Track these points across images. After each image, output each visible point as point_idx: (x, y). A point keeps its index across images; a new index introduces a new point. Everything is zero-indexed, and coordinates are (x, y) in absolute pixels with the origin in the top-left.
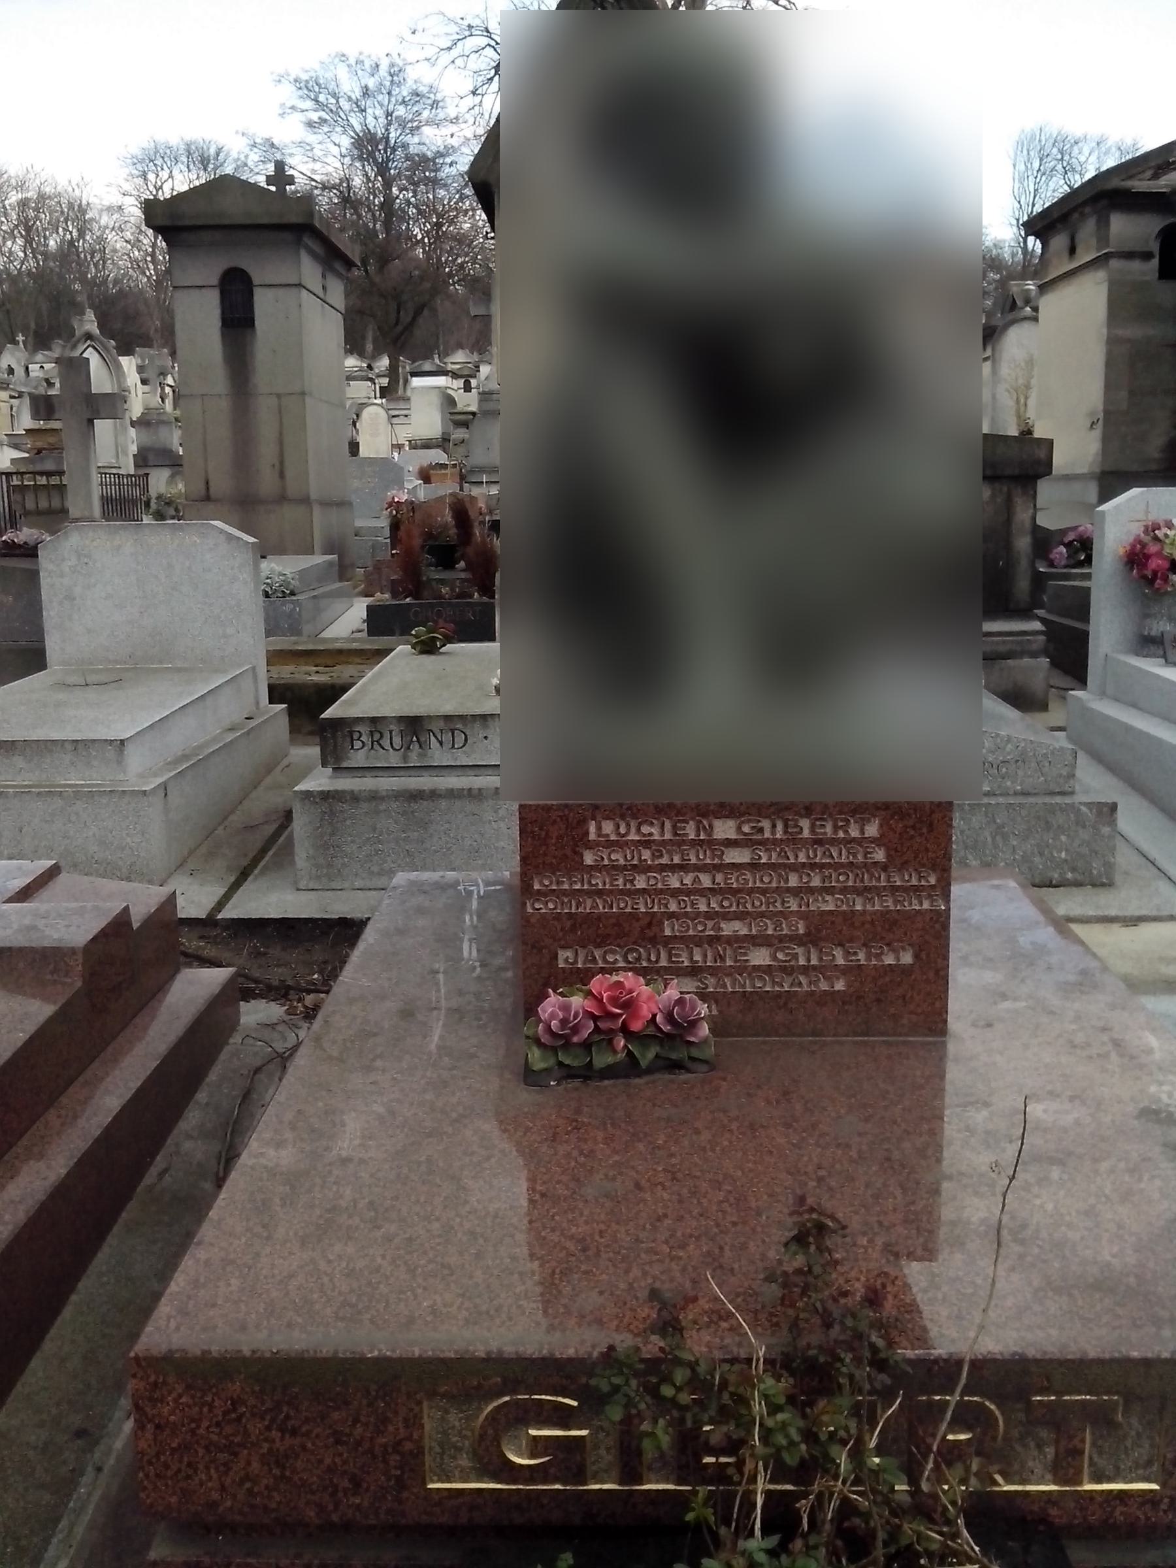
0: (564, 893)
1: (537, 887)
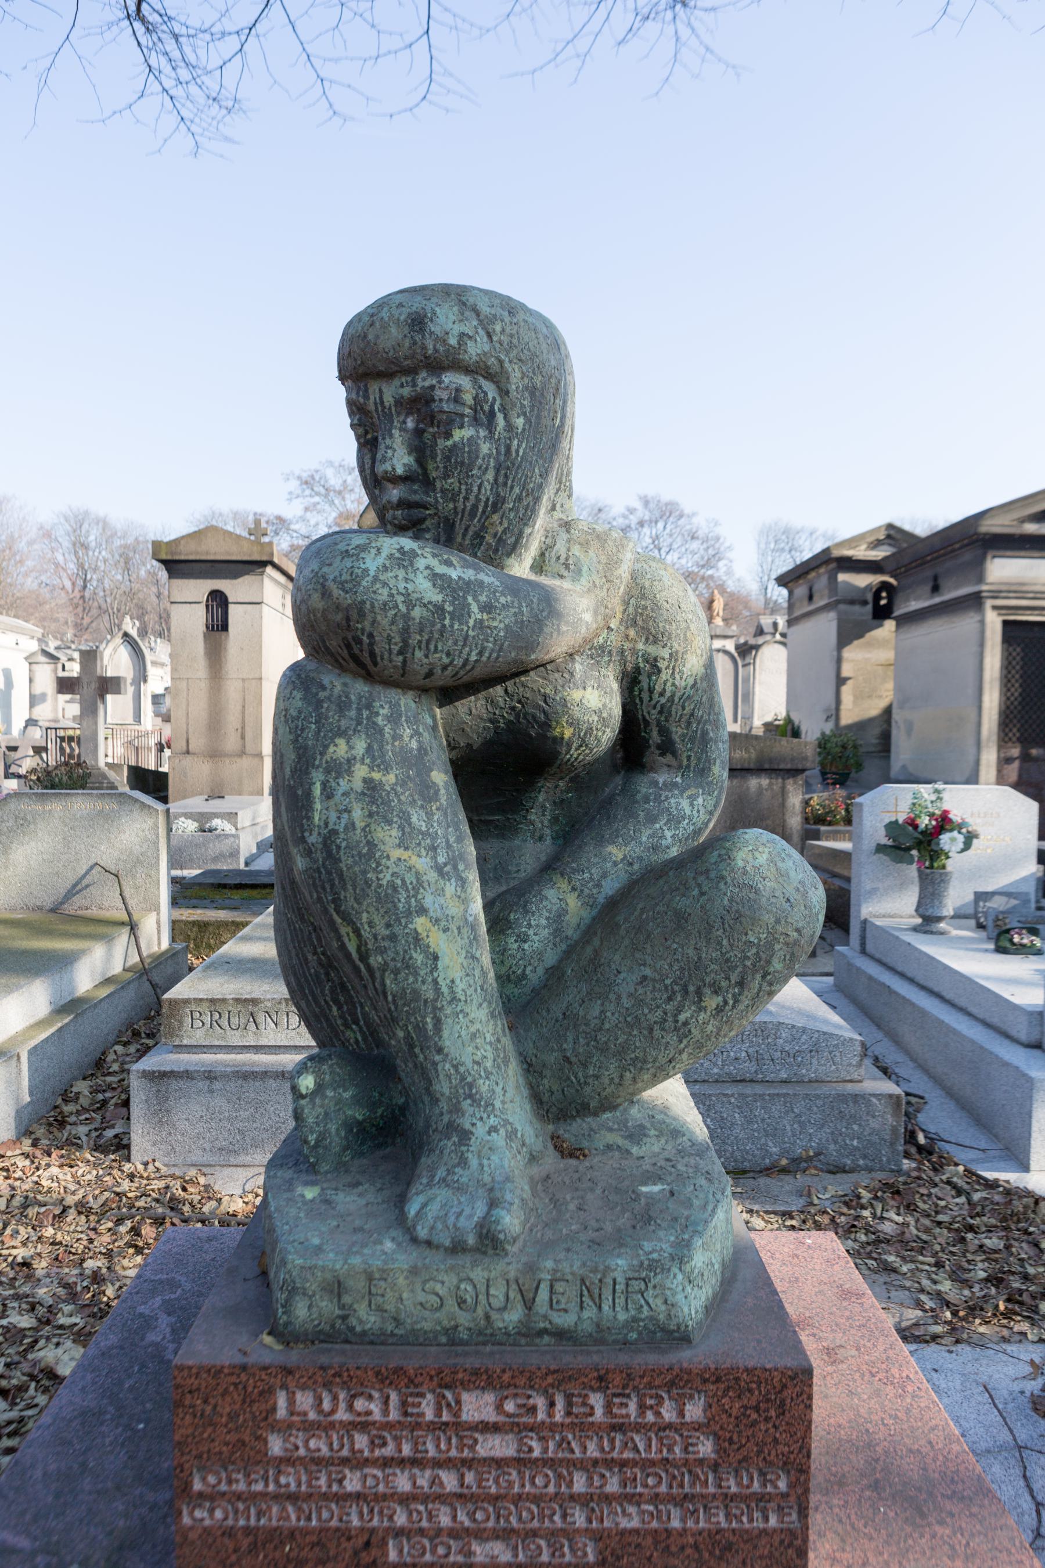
0: (239, 1496)
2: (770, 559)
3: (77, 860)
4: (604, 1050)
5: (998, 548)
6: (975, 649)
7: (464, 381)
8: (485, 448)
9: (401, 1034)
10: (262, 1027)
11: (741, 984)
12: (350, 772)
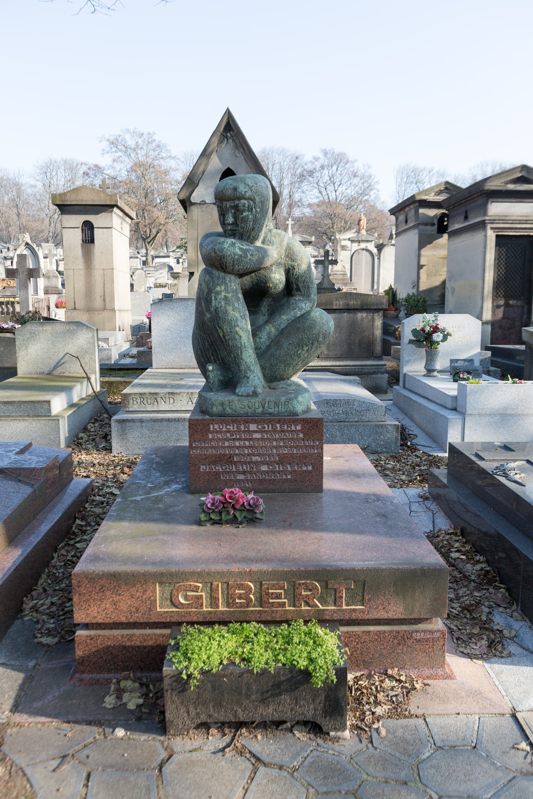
0: (203, 447)
1: (194, 445)
2: (403, 188)
3: (59, 352)
4: (280, 362)
5: (494, 197)
6: (483, 250)
7: (245, 202)
8: (250, 217)
9: (233, 356)
10: (159, 403)
11: (312, 344)
12: (221, 294)
